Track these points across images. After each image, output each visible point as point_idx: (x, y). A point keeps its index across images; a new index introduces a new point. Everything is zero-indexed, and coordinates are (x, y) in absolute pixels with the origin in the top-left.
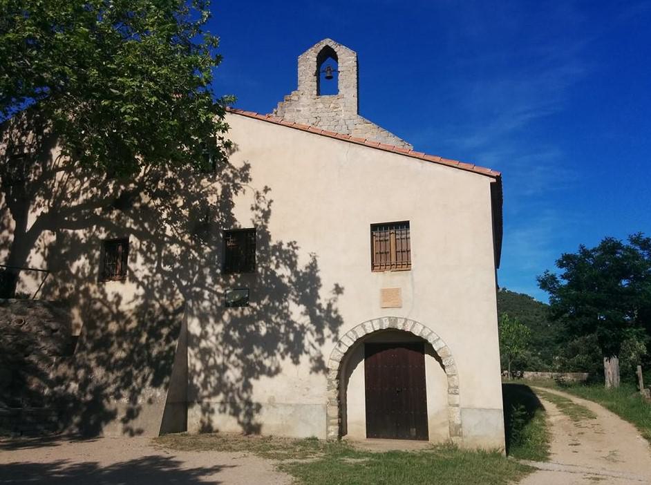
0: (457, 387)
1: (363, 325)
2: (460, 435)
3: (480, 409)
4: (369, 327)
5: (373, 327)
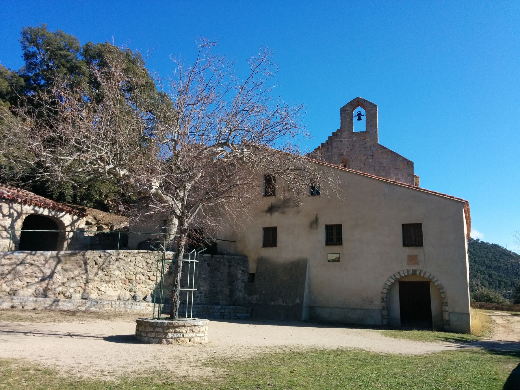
0: (447, 303)
1: (399, 273)
2: (449, 325)
3: (459, 313)
4: (402, 273)
5: (404, 274)
